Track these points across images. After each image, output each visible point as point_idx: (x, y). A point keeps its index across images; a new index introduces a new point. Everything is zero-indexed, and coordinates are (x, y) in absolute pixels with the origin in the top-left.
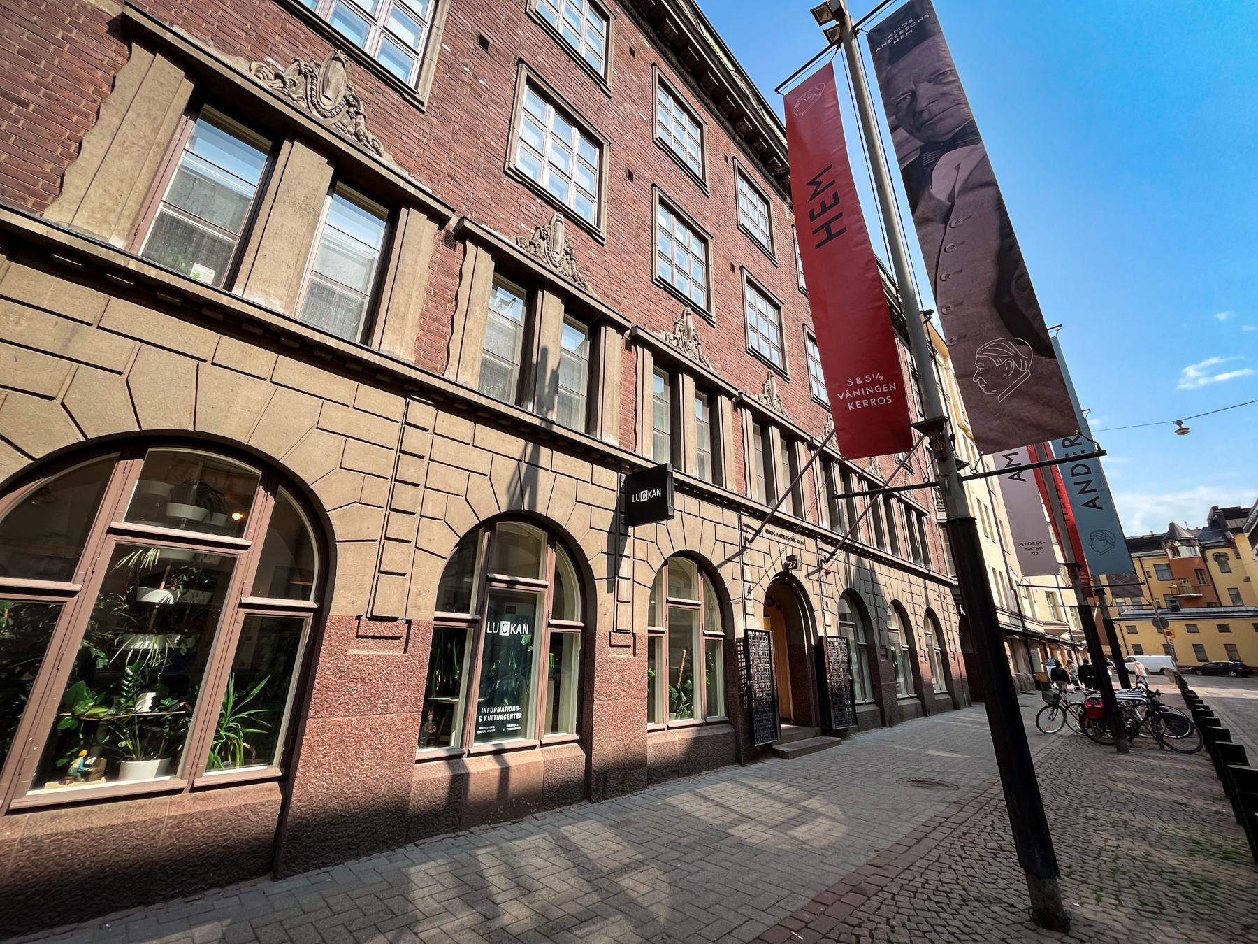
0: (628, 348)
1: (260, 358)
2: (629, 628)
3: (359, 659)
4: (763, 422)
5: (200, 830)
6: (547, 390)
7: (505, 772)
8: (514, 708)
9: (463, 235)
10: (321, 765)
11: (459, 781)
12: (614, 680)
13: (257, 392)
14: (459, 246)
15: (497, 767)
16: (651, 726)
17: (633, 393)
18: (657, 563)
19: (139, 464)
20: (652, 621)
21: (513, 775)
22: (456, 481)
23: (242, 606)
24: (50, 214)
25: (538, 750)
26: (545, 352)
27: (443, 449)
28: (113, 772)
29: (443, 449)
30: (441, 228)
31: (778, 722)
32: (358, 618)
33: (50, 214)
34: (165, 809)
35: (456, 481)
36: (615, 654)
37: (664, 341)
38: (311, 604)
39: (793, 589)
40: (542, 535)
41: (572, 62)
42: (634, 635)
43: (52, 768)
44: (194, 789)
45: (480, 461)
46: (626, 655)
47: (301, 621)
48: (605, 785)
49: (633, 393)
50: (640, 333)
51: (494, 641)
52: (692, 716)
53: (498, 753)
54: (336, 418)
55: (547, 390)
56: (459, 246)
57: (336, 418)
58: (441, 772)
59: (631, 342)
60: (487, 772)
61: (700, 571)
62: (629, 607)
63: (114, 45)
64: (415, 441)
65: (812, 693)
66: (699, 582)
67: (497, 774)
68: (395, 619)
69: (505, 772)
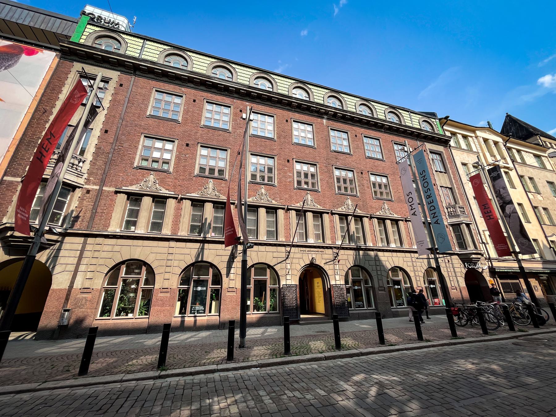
0: (370, 220)
1: (140, 242)
2: (382, 286)
3: (160, 297)
4: (382, 220)
5: (136, 325)
6: (207, 229)
7: (195, 321)
8: (202, 307)
9: (289, 209)
10: (154, 316)
11: (183, 322)
12: (229, 300)
13: (139, 249)
14: (288, 212)
15: (194, 319)
16: (392, 307)
17: (333, 227)
18: (423, 271)
19: (124, 266)
20: (425, 284)
21: (197, 321)
22: (182, 257)
23: (210, 287)
24: (179, 234)
25: (206, 317)
26: (206, 219)
27: (178, 251)
28: (127, 315)
29: (178, 251)
30: (176, 200)
31: (299, 313)
32: (160, 288)
33: (109, 230)
34: (134, 320)
35: (182, 257)
36: (453, 291)
37: (380, 215)
38: (220, 286)
39: (319, 269)
40: (433, 270)
41: (216, 131)
42: (384, 287)
43: (118, 314)
44: (135, 318)
45: (187, 251)
46: (455, 291)
47: (219, 289)
48: (224, 326)
49: (333, 227)
50: (407, 219)
51: (355, 290)
52: (265, 311)
53: (195, 317)
54: (155, 250)
55: (207, 229)
56: (182, 202)
57: (155, 250)
58: (192, 319)
59: (287, 211)
60: (191, 320)
61: (400, 271)
62: (234, 281)
63: (115, 195)
64: (171, 251)
65: (329, 304)
66: (400, 273)
67: (193, 321)
68: (168, 288)
69: (195, 321)
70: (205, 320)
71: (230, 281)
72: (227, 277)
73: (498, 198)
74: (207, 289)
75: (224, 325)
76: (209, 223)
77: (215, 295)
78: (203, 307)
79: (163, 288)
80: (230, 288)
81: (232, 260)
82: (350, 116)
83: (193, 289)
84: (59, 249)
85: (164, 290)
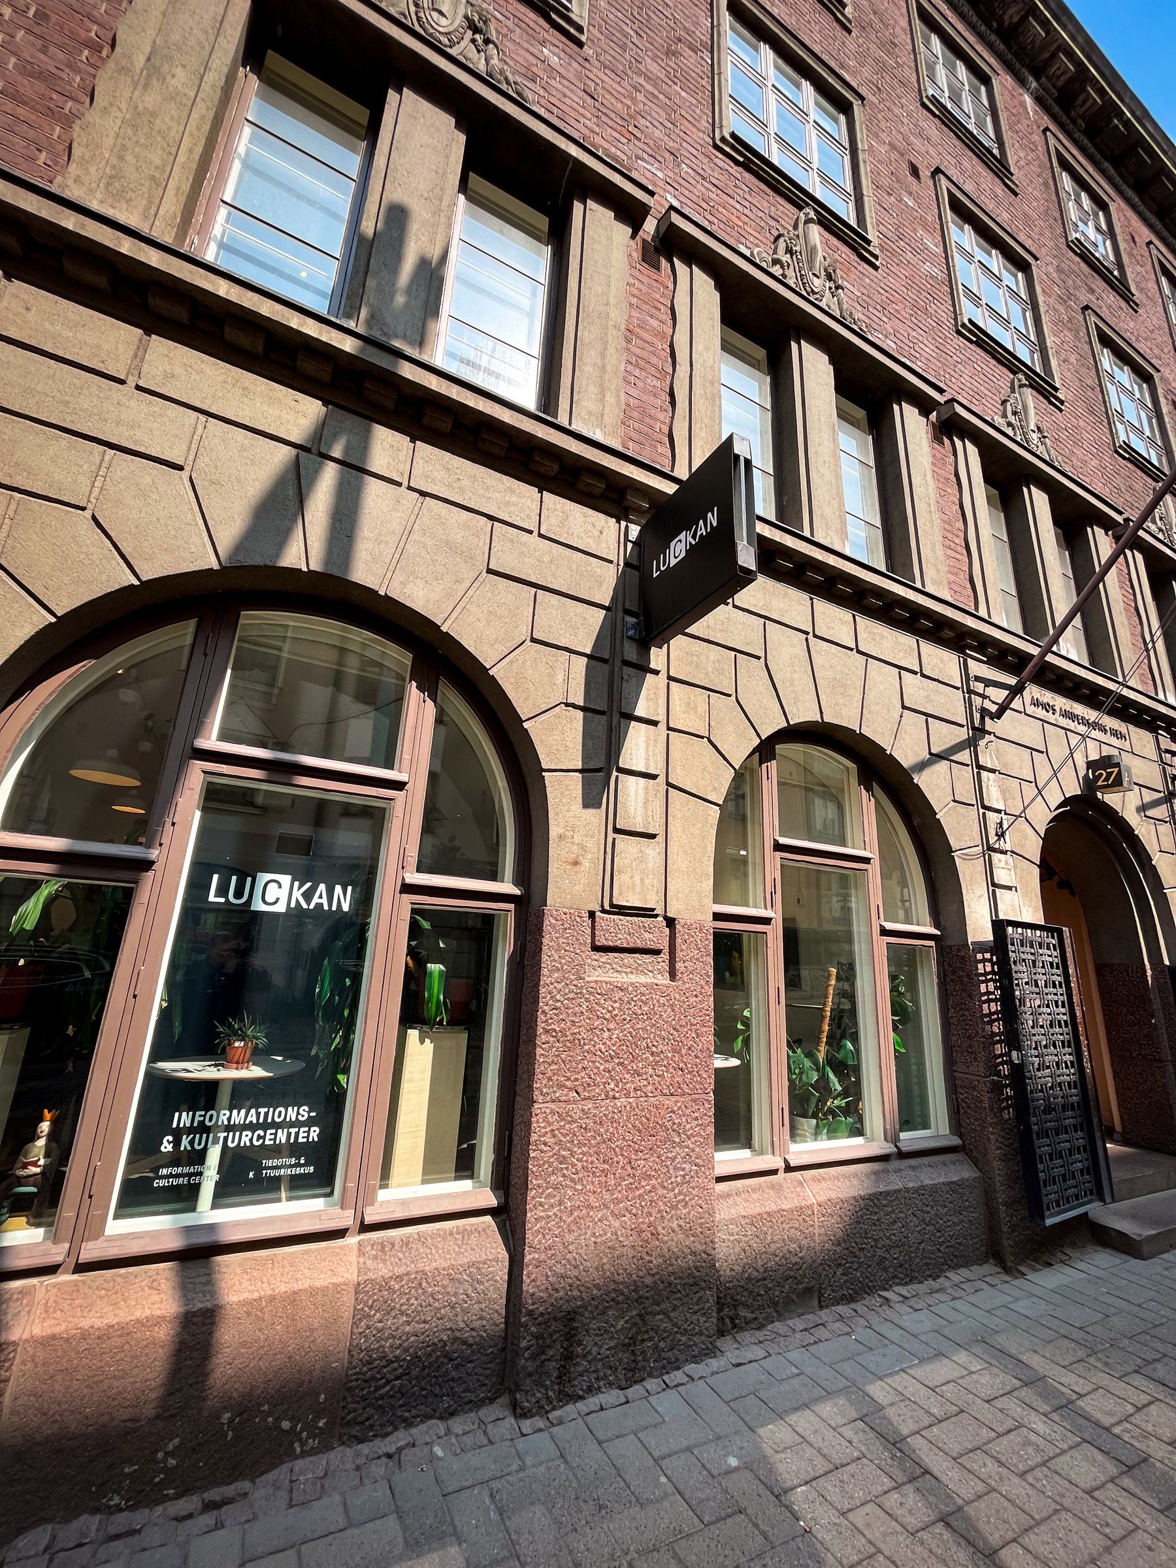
6: (400, 299)
47: (488, 920)
48: (568, 1357)
62: (653, 850)
67: (164, 1333)
70: (337, 1288)
71: (623, 842)
72: (591, 800)
73: (289, 802)
74: (364, 901)
75: (570, 1336)
76: (423, 263)
77: (447, 977)
78: (304, 1112)
79: (122, 382)
80: (621, 910)
81: (631, 652)
82: (1127, 123)
83: (197, 885)
84: (985, 1444)
85: (228, 292)
